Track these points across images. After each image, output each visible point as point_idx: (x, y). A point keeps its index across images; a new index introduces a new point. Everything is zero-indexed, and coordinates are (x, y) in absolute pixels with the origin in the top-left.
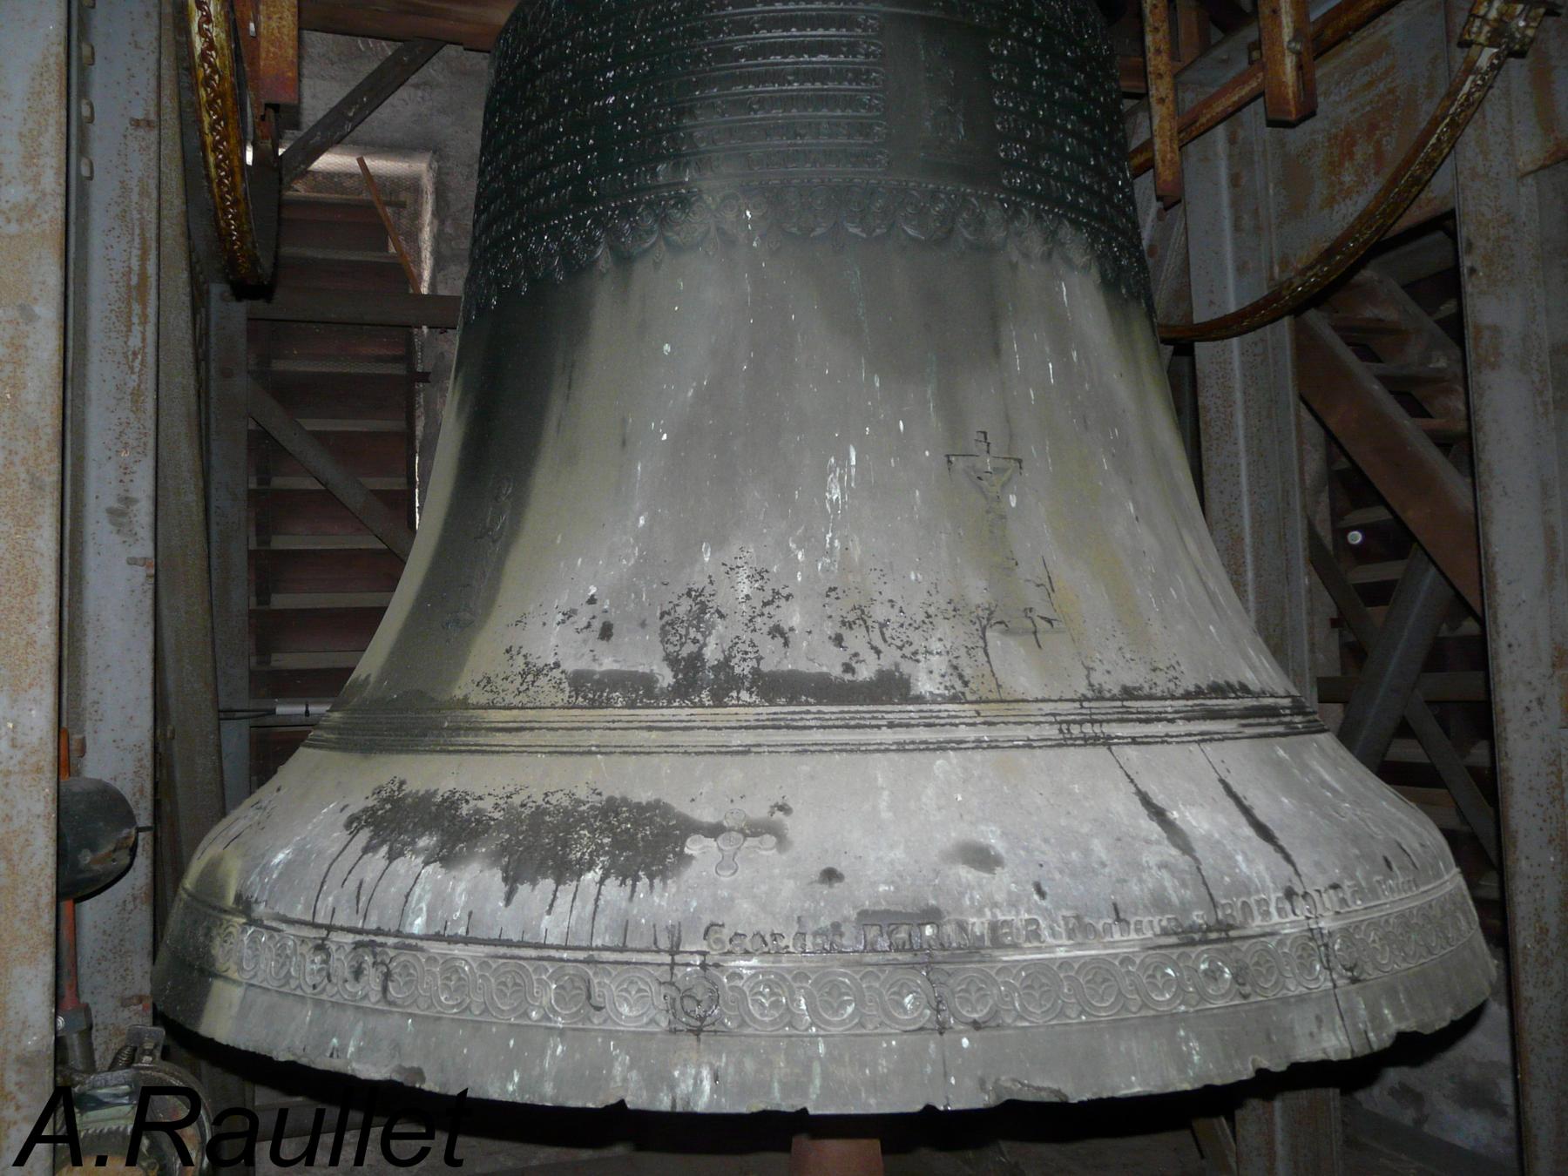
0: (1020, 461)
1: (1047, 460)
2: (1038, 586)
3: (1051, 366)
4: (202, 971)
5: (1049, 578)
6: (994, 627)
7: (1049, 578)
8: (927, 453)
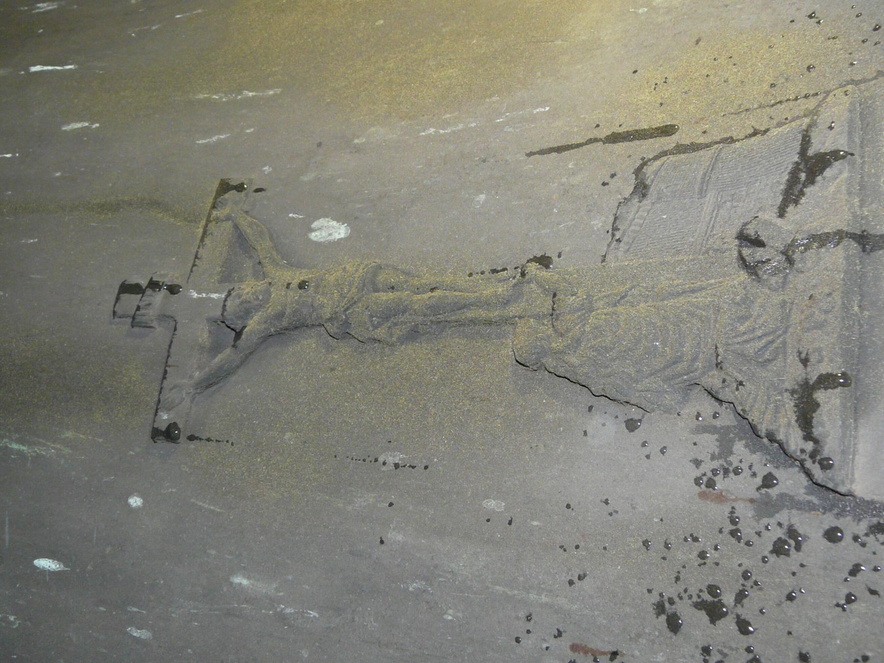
0: (225, 187)
1: (249, 103)
2: (641, 189)
3: (38, 68)
4: (870, 528)
5: (614, 138)
6: (830, 448)
7: (614, 138)
8: (135, 501)
